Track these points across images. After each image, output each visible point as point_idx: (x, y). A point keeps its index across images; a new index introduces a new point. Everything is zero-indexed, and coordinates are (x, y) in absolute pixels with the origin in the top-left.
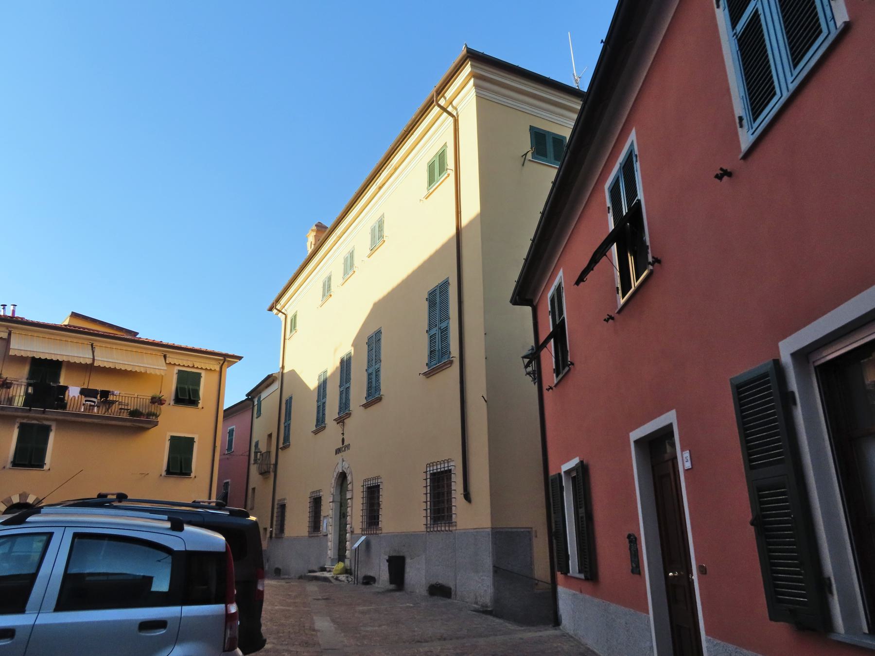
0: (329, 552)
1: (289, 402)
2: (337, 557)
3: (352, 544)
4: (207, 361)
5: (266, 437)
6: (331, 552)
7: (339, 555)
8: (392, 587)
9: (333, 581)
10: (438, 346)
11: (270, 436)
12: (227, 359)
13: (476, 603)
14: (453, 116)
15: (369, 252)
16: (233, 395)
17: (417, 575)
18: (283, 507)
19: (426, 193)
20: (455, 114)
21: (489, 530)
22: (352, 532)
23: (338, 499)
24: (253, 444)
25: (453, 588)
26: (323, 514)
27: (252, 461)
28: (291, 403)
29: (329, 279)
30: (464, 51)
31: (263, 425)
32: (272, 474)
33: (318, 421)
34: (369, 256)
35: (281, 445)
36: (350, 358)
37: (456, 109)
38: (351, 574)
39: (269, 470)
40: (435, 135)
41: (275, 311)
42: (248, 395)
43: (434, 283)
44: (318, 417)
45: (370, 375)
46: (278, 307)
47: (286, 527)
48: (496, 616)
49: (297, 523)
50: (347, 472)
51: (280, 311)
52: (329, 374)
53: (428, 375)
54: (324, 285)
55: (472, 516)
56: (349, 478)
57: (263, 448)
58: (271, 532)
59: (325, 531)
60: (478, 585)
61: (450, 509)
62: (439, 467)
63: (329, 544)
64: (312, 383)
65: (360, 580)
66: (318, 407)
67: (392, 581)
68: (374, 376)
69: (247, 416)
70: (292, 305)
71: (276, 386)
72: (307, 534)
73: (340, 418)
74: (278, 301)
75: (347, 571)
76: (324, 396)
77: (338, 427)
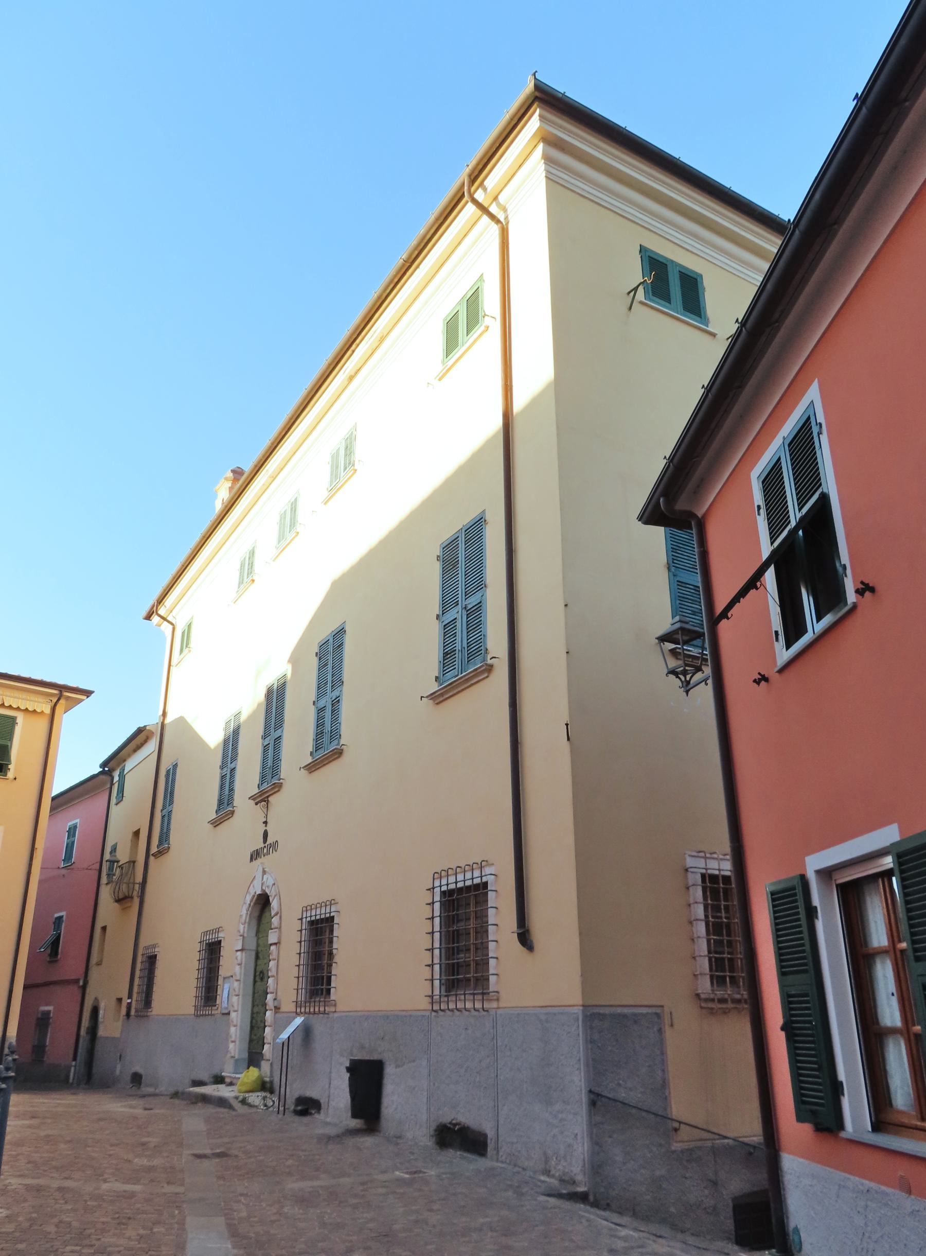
0: (231, 1046)
1: (171, 775)
2: (245, 1055)
3: (277, 1032)
4: (24, 695)
5: (130, 836)
6: (236, 1047)
7: (251, 1054)
8: (356, 1123)
9: (236, 1104)
10: (460, 641)
11: (137, 834)
12: (65, 695)
13: (547, 1172)
14: (498, 221)
15: (326, 494)
16: (74, 765)
17: (405, 1100)
18: (152, 960)
19: (439, 368)
20: (501, 217)
21: (578, 1010)
22: (277, 1008)
23: (252, 945)
24: (108, 849)
25: (491, 1134)
26: (223, 972)
27: (104, 879)
28: (174, 774)
29: (252, 553)
30: (530, 86)
31: (127, 814)
32: (136, 901)
33: (220, 802)
34: (326, 502)
35: (154, 849)
36: (284, 684)
37: (505, 210)
38: (272, 1092)
39: (132, 894)
40: (464, 259)
41: (156, 619)
42: (104, 765)
43: (453, 524)
44: (221, 795)
45: (321, 711)
46: (162, 611)
47: (156, 997)
48: (596, 1205)
49: (177, 988)
50: (271, 892)
51: (164, 619)
52: (243, 717)
53: (438, 698)
54: (242, 565)
55: (538, 978)
56: (274, 904)
57: (123, 856)
58: (129, 1005)
59: (225, 1005)
60: (554, 1133)
61: (483, 964)
62: (460, 877)
63: (233, 1029)
64: (214, 737)
65: (291, 1105)
66: (223, 777)
67: (356, 1112)
68: (328, 714)
69: (97, 804)
70: (181, 608)
71: (151, 747)
72: (192, 1011)
73: (261, 793)
74: (160, 600)
75: (264, 1086)
76: (234, 758)
77: (257, 812)
